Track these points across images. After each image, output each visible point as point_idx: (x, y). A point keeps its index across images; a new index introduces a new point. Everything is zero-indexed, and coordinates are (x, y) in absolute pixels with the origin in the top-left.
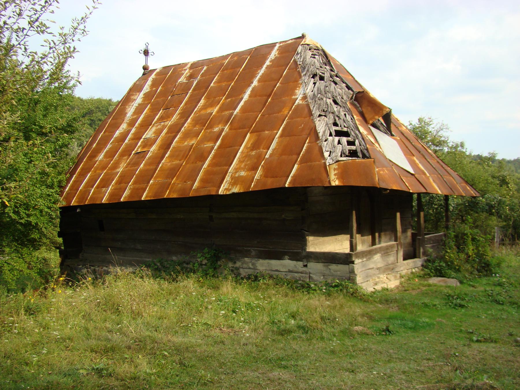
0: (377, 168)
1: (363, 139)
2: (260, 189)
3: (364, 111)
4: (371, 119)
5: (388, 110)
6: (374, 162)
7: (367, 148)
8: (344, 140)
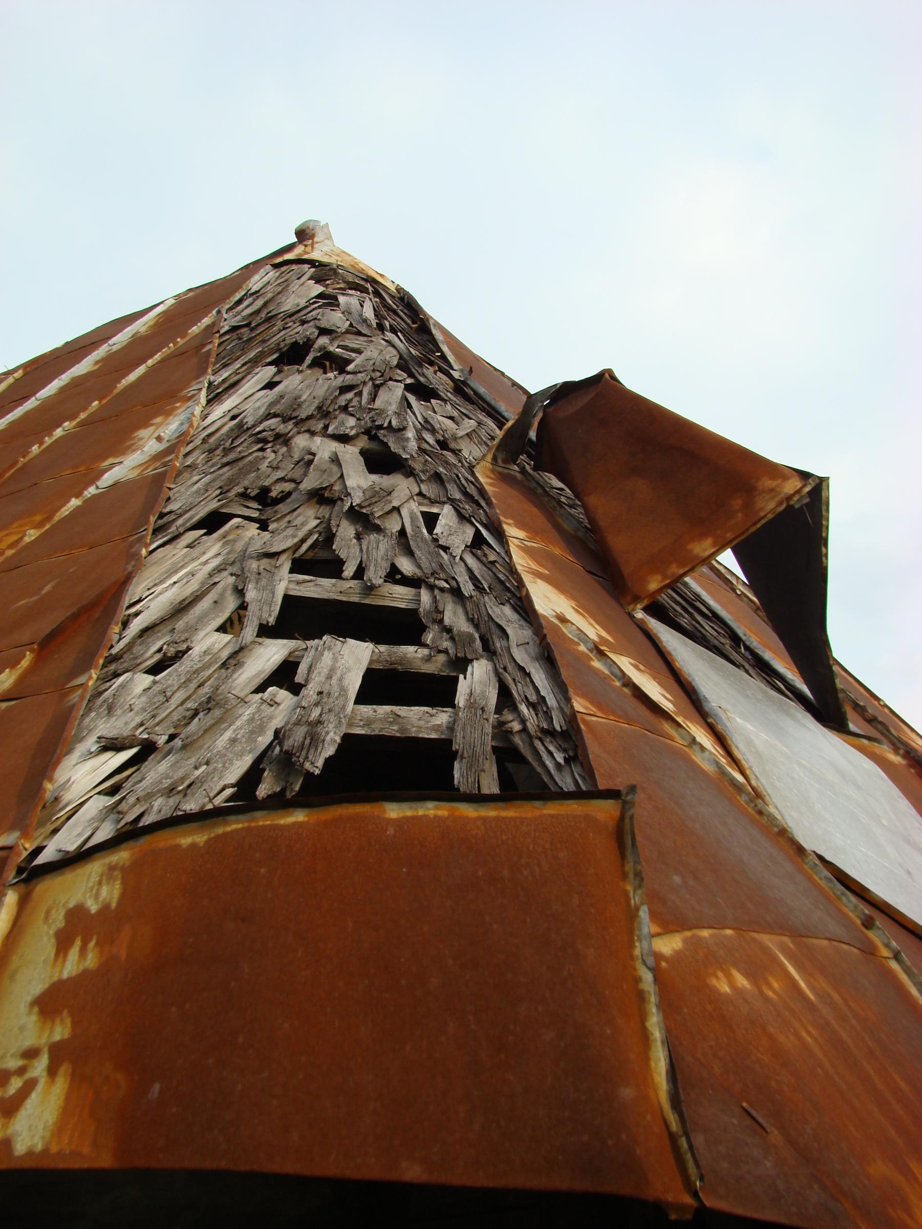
0: (669, 923)
1: (548, 659)
2: (461, 1176)
3: (604, 505)
4: (656, 564)
5: (792, 486)
6: (622, 836)
7: (572, 718)
8: (354, 657)
